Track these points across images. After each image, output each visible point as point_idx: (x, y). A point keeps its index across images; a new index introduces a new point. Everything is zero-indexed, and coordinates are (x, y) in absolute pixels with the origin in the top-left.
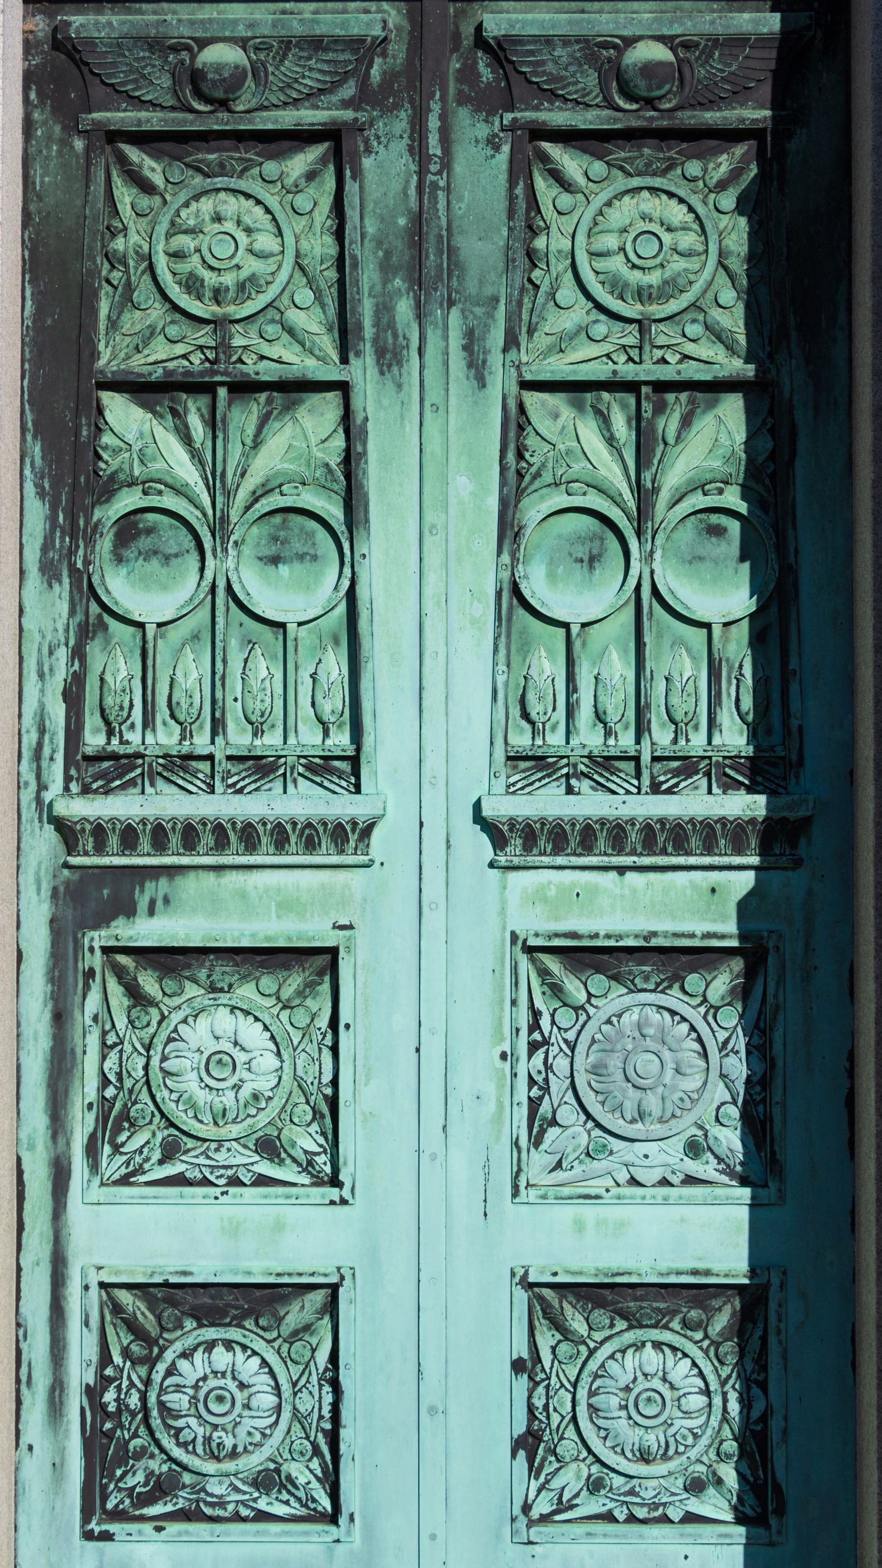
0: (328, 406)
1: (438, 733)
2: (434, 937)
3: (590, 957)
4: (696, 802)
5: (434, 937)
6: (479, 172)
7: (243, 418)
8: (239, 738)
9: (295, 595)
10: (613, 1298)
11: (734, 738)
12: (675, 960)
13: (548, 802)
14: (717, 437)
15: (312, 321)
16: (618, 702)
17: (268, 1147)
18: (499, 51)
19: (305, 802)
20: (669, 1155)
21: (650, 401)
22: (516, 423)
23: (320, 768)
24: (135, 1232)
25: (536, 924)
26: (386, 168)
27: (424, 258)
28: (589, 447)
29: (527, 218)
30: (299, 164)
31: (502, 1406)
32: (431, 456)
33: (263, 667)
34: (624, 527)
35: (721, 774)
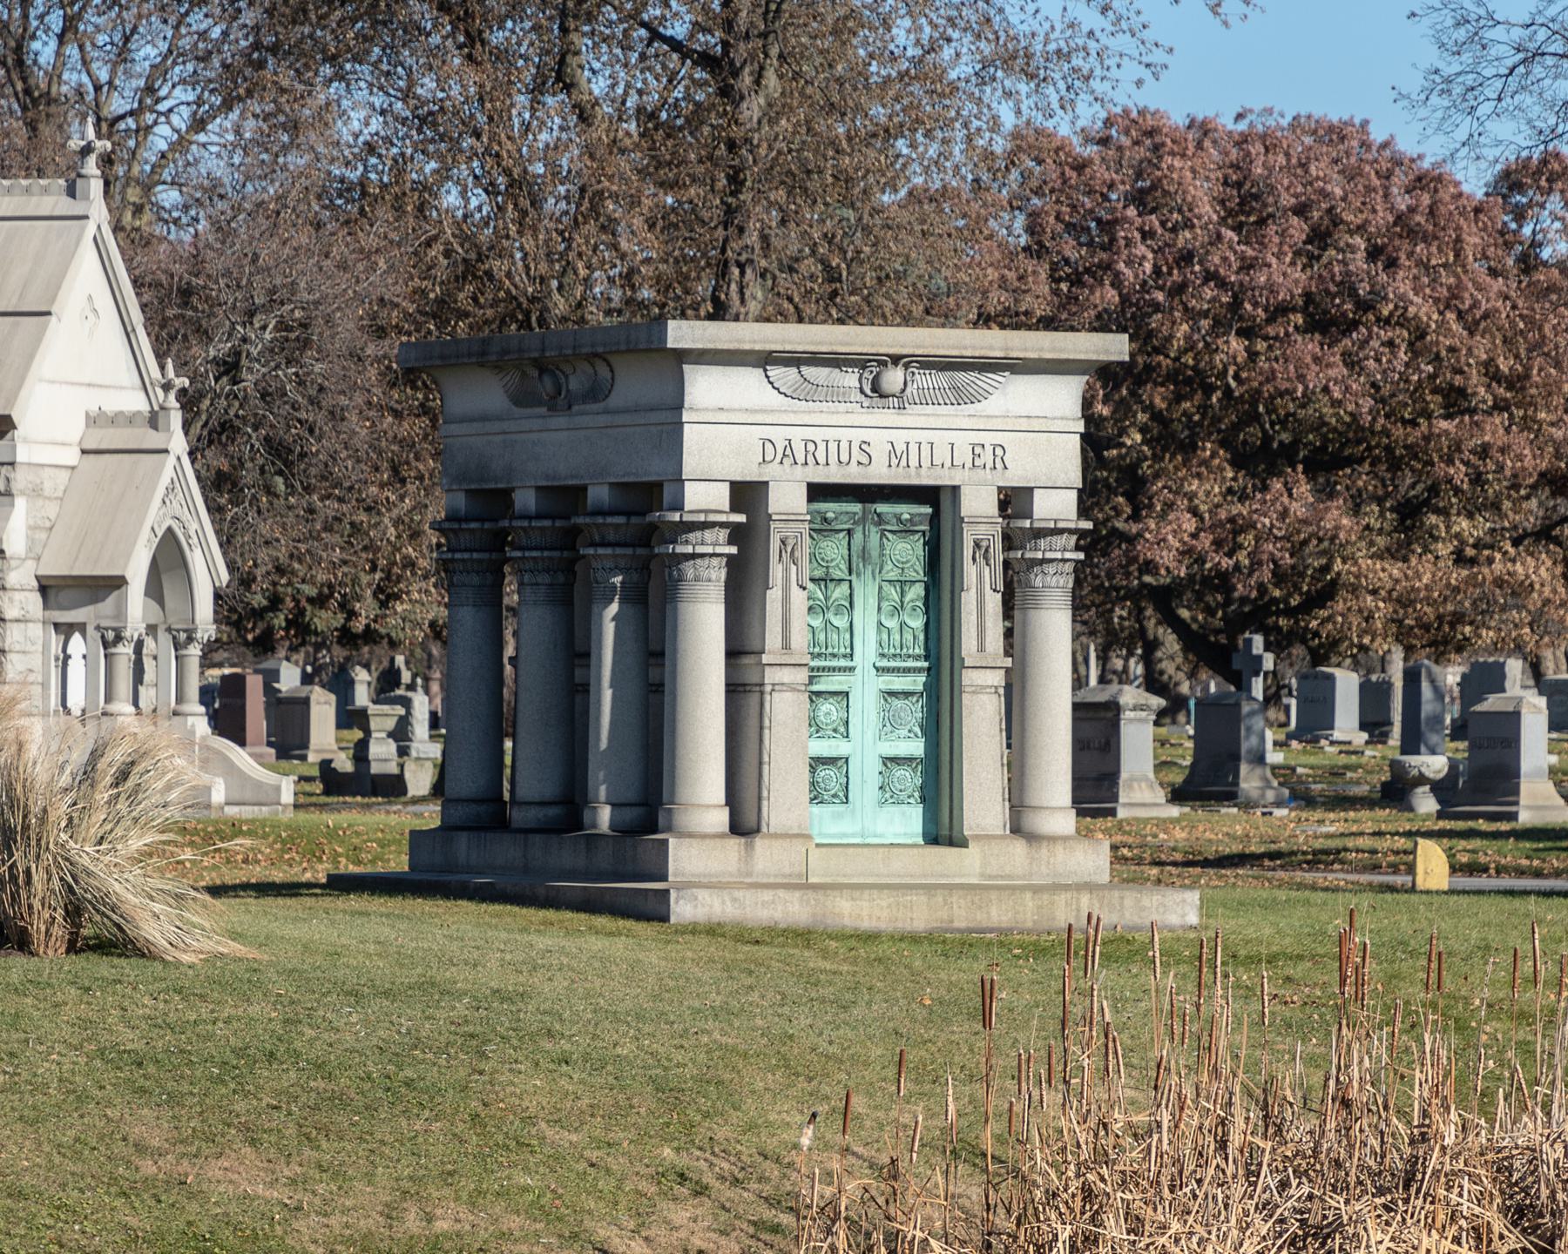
0: (845, 587)
1: (867, 651)
2: (866, 688)
3: (892, 694)
4: (910, 664)
5: (866, 688)
6: (874, 537)
7: (831, 586)
8: (830, 650)
9: (841, 622)
10: (896, 760)
11: (919, 651)
12: (907, 694)
13: (884, 663)
14: (917, 591)
15: (844, 567)
16: (897, 644)
17: (835, 730)
18: (879, 515)
19: (843, 663)
20: (904, 732)
21: (903, 584)
22: (880, 588)
23: (845, 656)
24: (821, 748)
25: (883, 687)
26: (858, 537)
27: (864, 555)
28: (893, 593)
29: (882, 546)
30: (841, 535)
31: (876, 781)
32: (866, 594)
33: (835, 636)
34: (898, 610)
35: (917, 658)
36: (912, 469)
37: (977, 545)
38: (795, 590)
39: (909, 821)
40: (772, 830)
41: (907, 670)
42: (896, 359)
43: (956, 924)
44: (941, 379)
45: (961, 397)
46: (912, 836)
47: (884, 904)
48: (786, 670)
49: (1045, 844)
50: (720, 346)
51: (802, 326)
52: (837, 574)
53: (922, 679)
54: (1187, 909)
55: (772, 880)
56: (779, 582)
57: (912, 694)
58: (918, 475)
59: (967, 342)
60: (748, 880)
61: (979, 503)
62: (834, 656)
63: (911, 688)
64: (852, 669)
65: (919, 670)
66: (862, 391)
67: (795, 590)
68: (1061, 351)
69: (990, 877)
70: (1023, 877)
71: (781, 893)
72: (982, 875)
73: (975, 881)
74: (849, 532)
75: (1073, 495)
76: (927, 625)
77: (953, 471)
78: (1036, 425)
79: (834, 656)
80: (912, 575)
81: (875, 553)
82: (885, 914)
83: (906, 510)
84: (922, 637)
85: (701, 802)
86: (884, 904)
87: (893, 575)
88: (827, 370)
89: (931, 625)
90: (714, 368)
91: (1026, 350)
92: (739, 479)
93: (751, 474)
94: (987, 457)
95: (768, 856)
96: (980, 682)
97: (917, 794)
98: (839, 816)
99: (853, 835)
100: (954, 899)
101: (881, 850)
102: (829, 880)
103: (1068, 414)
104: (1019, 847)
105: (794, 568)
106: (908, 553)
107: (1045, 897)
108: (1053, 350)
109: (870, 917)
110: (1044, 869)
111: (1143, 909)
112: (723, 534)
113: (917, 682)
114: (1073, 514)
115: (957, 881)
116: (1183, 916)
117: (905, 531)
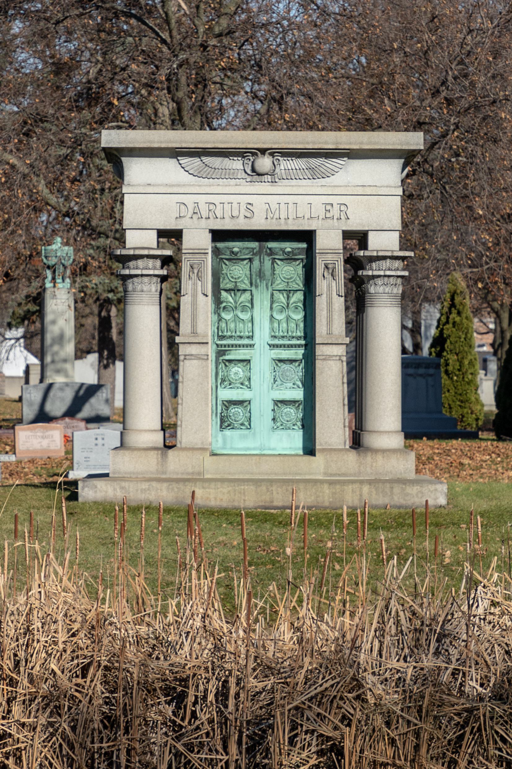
0: (249, 293)
1: (263, 333)
2: (262, 358)
3: (280, 361)
5: (262, 358)
6: (268, 263)
7: (239, 294)
8: (238, 334)
9: (245, 316)
10: (284, 402)
11: (300, 333)
12: (292, 361)
13: (276, 342)
14: (300, 296)
15: (247, 282)
17: (242, 384)
18: (270, 249)
19: (246, 342)
21: (289, 292)
22: (272, 295)
23: (248, 337)
24: (226, 394)
25: (274, 357)
26: (256, 263)
27: (261, 274)
28: (281, 298)
29: (273, 269)
30: (245, 262)
31: (271, 415)
35: (298, 338)
36: (282, 221)
37: (326, 267)
38: (201, 297)
39: (294, 440)
40: (183, 445)
41: (295, 346)
42: (263, 151)
43: (275, 504)
44: (301, 163)
45: (315, 174)
46: (296, 449)
47: (225, 491)
48: (194, 346)
49: (369, 454)
50: (137, 145)
51: (150, 131)
52: (242, 286)
53: (301, 351)
54: (439, 494)
55: (180, 476)
56: (190, 292)
57: (295, 361)
58: (286, 224)
59: (310, 140)
60: (164, 476)
61: (329, 241)
62: (241, 337)
63: (293, 357)
64: (252, 346)
65: (299, 346)
66: (246, 172)
67: (201, 297)
68: (375, 143)
69: (331, 475)
70: (355, 475)
71: (154, 484)
72: (325, 474)
73: (320, 477)
74: (250, 260)
75: (397, 234)
76: (305, 317)
77: (311, 221)
78: (368, 191)
79: (241, 337)
80: (295, 286)
81: (268, 273)
82: (225, 497)
83: (288, 246)
84: (302, 325)
85: (370, 430)
86: (225, 491)
87: (281, 287)
88: (220, 159)
89: (308, 318)
90: (143, 159)
91: (350, 143)
92: (162, 228)
93: (171, 225)
94: (335, 212)
95: (176, 462)
96: (328, 353)
97: (299, 424)
98: (245, 437)
99: (254, 449)
100: (274, 488)
101: (254, 458)
102: (218, 476)
103: (392, 184)
104: (352, 457)
105: (200, 283)
106: (291, 273)
107: (338, 487)
108: (370, 143)
109: (215, 499)
110: (368, 470)
111: (407, 495)
112: (158, 263)
113: (299, 353)
114: (397, 247)
115: (307, 477)
116: (436, 499)
117: (289, 258)
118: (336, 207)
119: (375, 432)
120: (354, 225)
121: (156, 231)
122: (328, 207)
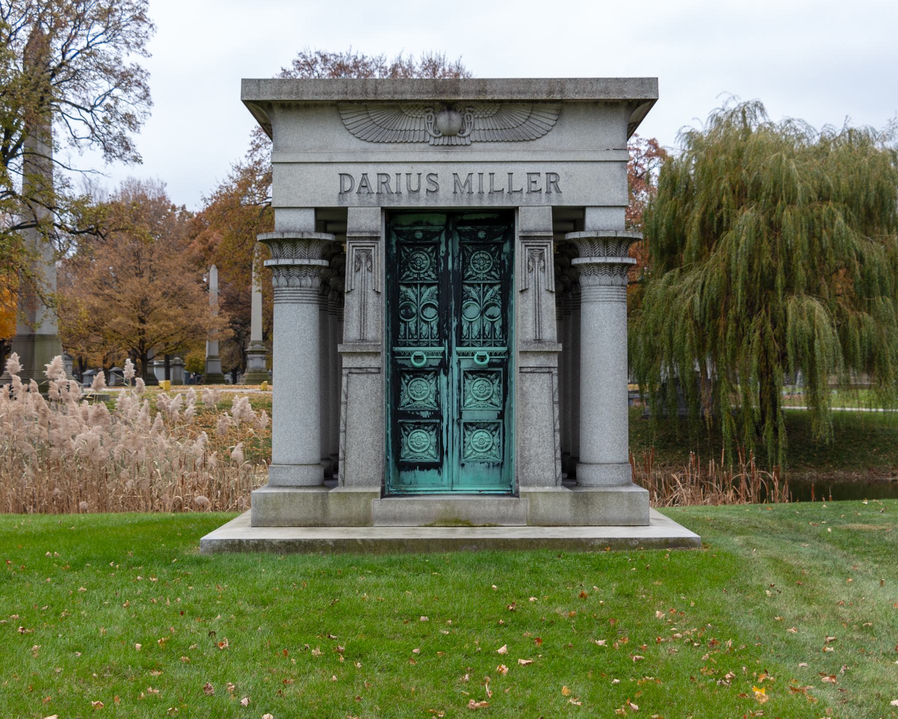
25: (630, 390)
61: (534, 218)
94: (542, 184)
118: (543, 176)
119: (591, 464)
120: (569, 199)
121: (312, 212)
122: (534, 178)
